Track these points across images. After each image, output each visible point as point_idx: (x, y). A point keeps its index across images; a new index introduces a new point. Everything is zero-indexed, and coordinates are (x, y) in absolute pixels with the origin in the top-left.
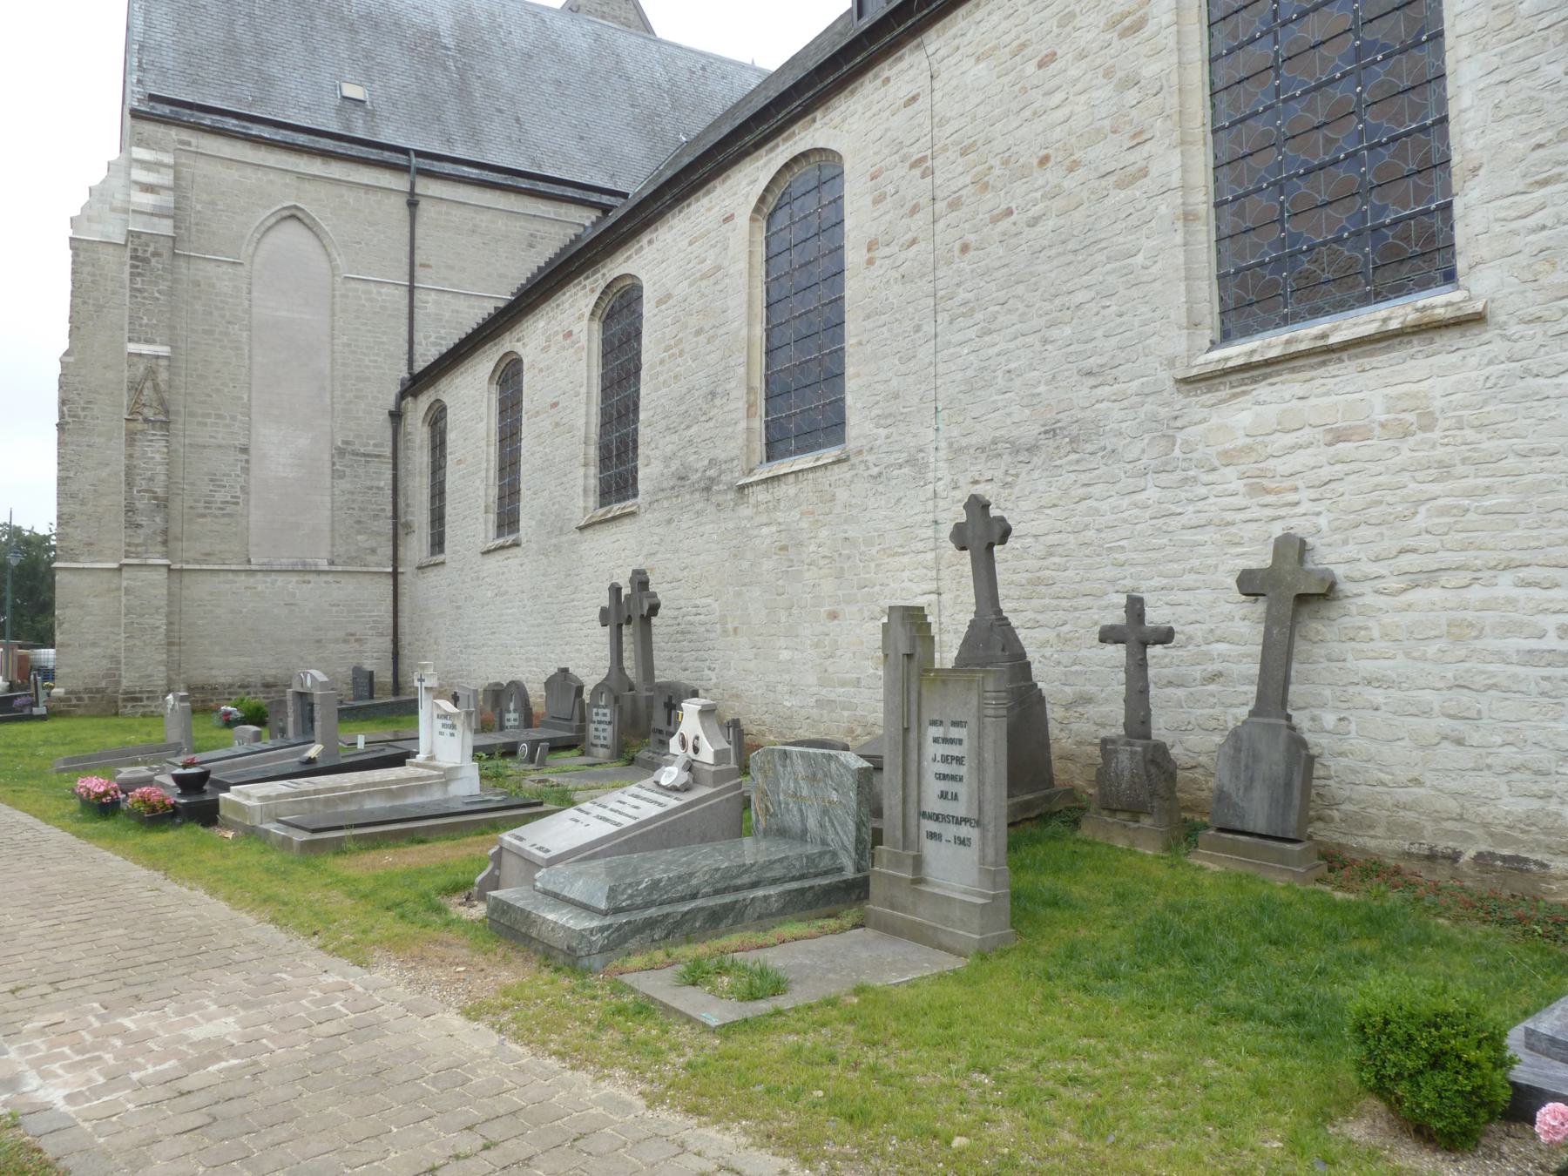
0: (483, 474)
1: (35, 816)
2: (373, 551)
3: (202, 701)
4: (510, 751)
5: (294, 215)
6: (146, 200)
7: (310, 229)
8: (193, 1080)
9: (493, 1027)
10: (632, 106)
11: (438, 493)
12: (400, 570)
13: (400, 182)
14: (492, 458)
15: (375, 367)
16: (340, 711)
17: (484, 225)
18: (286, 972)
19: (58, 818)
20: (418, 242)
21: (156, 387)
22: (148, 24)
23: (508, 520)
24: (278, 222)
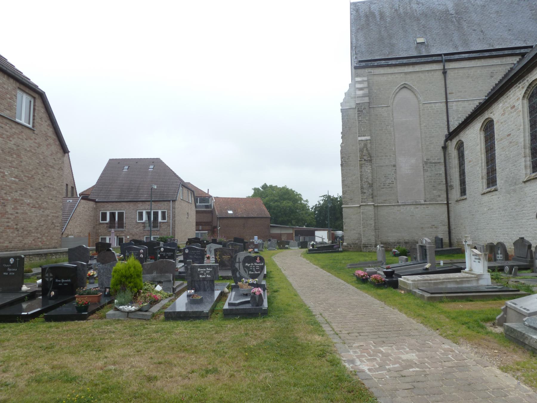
0: (480, 165)
1: (345, 281)
2: (439, 196)
3: (387, 247)
4: (501, 269)
5: (405, 87)
6: (360, 93)
7: (410, 90)
8: (405, 373)
9: (514, 376)
10: (531, 10)
11: (462, 173)
12: (450, 202)
13: (440, 66)
14: (483, 158)
15: (436, 132)
16: (436, 251)
17: (472, 73)
18: (430, 341)
19: (351, 282)
20: (448, 86)
21: (367, 149)
22: (357, 40)
23: (491, 180)
24: (400, 90)
